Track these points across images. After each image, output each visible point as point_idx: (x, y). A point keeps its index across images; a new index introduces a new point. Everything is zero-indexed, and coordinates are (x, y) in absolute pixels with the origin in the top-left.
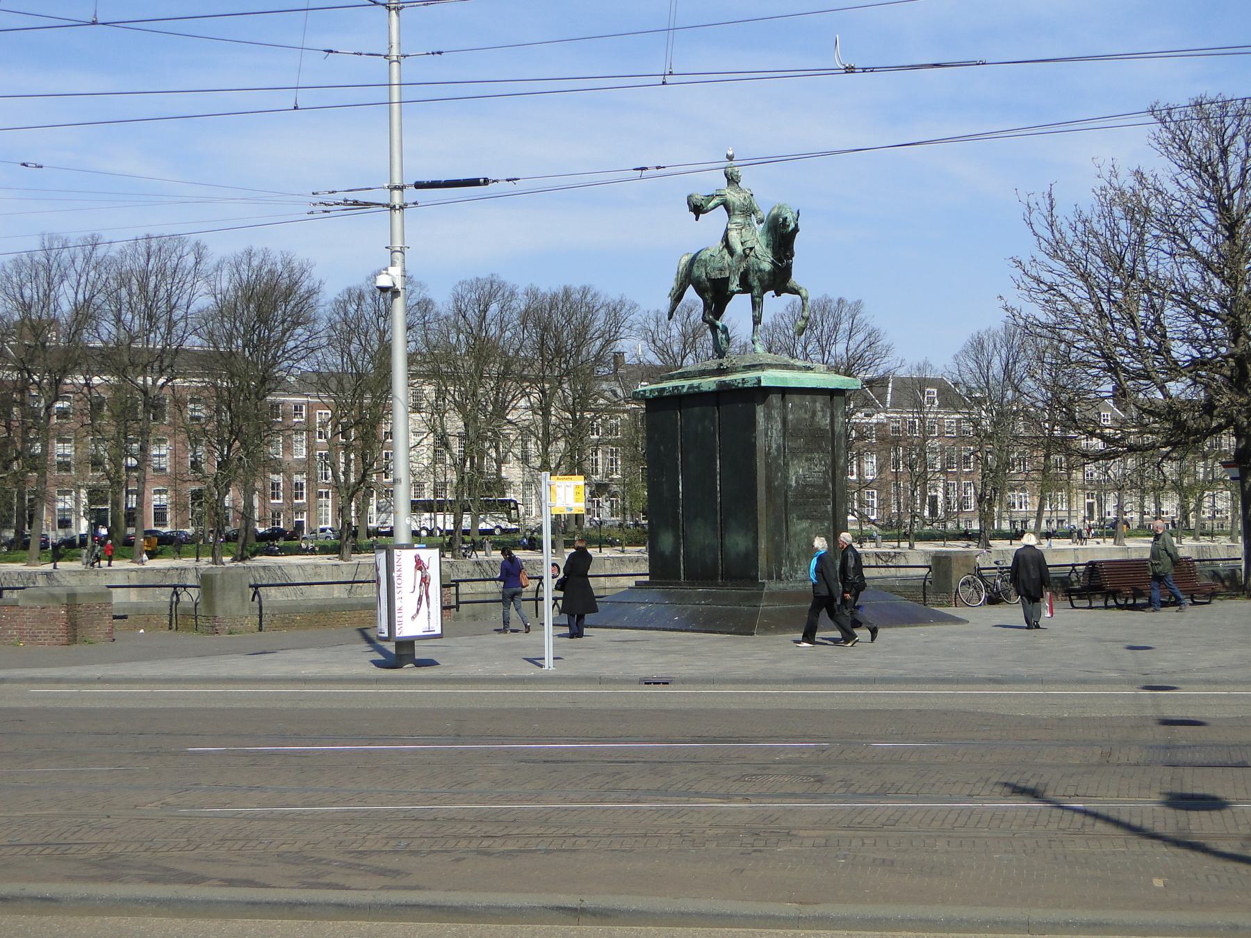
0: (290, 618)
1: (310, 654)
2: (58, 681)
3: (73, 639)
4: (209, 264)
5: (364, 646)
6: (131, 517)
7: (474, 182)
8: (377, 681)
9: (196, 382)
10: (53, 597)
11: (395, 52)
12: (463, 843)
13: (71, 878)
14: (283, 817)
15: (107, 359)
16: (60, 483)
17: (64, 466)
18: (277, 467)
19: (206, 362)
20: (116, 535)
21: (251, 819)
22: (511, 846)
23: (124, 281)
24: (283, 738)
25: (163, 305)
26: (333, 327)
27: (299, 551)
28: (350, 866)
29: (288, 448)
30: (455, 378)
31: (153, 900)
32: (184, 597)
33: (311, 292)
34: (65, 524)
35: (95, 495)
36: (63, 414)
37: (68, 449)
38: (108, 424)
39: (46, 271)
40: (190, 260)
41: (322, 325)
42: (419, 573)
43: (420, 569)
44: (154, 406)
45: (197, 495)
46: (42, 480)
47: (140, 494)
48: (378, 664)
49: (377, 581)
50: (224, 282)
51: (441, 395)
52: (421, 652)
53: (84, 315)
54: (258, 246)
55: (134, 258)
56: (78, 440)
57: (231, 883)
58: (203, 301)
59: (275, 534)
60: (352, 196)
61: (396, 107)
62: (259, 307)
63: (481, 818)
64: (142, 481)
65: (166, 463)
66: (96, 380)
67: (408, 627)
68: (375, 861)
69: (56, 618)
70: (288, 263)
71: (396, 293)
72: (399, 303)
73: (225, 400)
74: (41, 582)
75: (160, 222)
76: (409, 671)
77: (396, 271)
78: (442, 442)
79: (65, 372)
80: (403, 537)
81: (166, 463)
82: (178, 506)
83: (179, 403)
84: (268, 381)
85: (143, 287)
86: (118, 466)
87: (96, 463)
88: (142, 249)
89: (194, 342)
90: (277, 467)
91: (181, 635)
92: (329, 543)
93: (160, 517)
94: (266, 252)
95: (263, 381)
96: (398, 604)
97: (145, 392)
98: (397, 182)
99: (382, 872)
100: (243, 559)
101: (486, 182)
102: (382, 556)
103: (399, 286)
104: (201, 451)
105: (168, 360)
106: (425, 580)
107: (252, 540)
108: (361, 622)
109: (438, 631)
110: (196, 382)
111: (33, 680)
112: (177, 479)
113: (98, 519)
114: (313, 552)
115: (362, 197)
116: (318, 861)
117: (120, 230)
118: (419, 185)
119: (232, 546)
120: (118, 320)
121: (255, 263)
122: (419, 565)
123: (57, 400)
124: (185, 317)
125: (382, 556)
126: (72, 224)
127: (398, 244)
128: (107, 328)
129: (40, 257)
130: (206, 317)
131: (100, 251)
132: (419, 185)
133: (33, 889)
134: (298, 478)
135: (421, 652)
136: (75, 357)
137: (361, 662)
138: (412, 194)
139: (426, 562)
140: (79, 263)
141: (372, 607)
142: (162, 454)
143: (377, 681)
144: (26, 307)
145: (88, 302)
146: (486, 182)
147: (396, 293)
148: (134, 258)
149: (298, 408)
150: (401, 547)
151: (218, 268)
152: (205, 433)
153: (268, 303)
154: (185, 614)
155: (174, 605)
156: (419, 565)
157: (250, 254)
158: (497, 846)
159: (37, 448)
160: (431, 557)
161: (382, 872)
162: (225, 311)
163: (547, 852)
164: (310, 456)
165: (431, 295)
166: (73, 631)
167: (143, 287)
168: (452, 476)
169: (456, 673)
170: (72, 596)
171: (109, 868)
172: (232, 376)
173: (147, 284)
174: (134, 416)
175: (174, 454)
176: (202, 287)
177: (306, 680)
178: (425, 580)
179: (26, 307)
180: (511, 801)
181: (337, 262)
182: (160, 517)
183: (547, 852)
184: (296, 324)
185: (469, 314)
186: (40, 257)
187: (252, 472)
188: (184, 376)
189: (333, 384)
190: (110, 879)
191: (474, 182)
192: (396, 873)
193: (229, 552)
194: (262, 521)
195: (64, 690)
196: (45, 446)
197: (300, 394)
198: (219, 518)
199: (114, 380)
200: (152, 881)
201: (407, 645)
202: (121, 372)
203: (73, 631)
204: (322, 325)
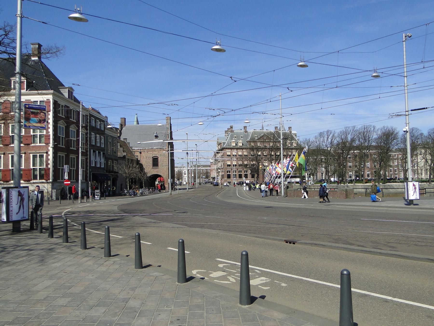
0: (389, 195)
1: (392, 202)
2: (342, 205)
3: (347, 198)
4: (376, 129)
5: (404, 201)
6: (362, 176)
7: (424, 108)
8: (405, 208)
9: (374, 151)
10: (343, 190)
11: (406, 85)
12: (412, 242)
13: (329, 242)
14: (375, 234)
15: (357, 148)
16: (349, 170)
17: (350, 167)
18: (391, 166)
19: (375, 147)
20: (360, 178)
21: (369, 233)
22: (423, 244)
23: (360, 133)
24: (380, 218)
25: (367, 138)
26: (402, 140)
27: (396, 182)
28: (385, 245)
29: (393, 163)
30: (429, 148)
31: (343, 248)
32: (368, 191)
33: (397, 133)
34: (351, 177)
35: (356, 172)
36: (350, 158)
37: (351, 164)
38: (358, 159)
39: (346, 133)
40: (373, 129)
41: (399, 139)
42: (20, 197)
43: (20, 196)
44: (366, 155)
45: (375, 172)
46: (346, 169)
47: (364, 172)
48: (406, 204)
49: (405, 188)
50: (379, 133)
51: (426, 152)
52: (415, 202)
53: (353, 140)
54: (386, 125)
55: (362, 129)
56: (352, 162)
57: (359, 246)
58: (375, 136)
59: (391, 179)
60: (397, 114)
61: (406, 94)
62: (386, 136)
63: (418, 237)
64: (364, 169)
65: (369, 166)
66: (355, 152)
67: (411, 198)
68: (390, 244)
69: (343, 194)
70: (392, 128)
71: (407, 132)
72: (408, 134)
73: (379, 154)
74: (346, 187)
75: (366, 122)
76: (412, 206)
77: (407, 128)
78: (426, 161)
79: (349, 150)
80: (410, 179)
81: (369, 166)
82: (372, 174)
83: (371, 155)
84: (388, 150)
85: (364, 134)
86: (360, 167)
87: (356, 166)
88: (363, 128)
89: (374, 144)
90: (391, 166)
91: (367, 197)
92: (402, 181)
93: (368, 176)
94: (387, 127)
95: (387, 150)
96: (409, 193)
97: (364, 153)
98: (407, 110)
99: (391, 247)
100: (384, 183)
101: (427, 108)
102: (405, 183)
103: (408, 130)
104: (376, 164)
105: (369, 148)
106: (415, 188)
107: (386, 180)
108: (402, 195)
109: (418, 198)
110: (374, 151)
111: (338, 205)
112: (371, 169)
113: (357, 176)
114: (399, 182)
115: (399, 114)
116: (378, 243)
117: (359, 125)
118: (412, 110)
119: (382, 181)
120: (359, 141)
121: (385, 128)
122: (414, 185)
123: (348, 155)
124: (372, 140)
125: (405, 183)
126: (350, 124)
127: (407, 122)
128: (357, 142)
129: (345, 131)
130: (376, 139)
131: (355, 129)
132: (412, 110)
133: (321, 243)
134: (395, 168)
135: (415, 202)
136: (352, 148)
137: (402, 204)
138: (410, 112)
139: (23, 193)
140: (352, 131)
141: (404, 193)
142: (368, 164)
143: (405, 208)
144: (342, 139)
145: (353, 138)
146: (427, 108)
147: (407, 132)
148: (362, 129)
149: (395, 155)
150: (410, 182)
151: (378, 130)
152: (376, 160)
153: (388, 136)
154: (368, 194)
155: (366, 192)
156: (414, 185)
157: (384, 127)
158: (420, 244)
159: (345, 164)
160: (417, 184)
161: (391, 247)
162: (380, 138)
163: (431, 246)
164: (398, 164)
165: (423, 132)
166: (347, 196)
167: (364, 134)
168: (428, 168)
169: (422, 207)
170: (346, 190)
171: (337, 241)
172: (381, 150)
173: (365, 134)
174: (363, 158)
175: (371, 164)
176: (375, 134)
177: (390, 207)
178: (415, 188)
179: (342, 139)
180: (426, 234)
181: (401, 127)
182: (368, 176)
183: (431, 246)
184: (394, 139)
185: (432, 135)
186: (345, 131)
187: (386, 167)
188: (372, 150)
189: (402, 150)
190: (336, 243)
191: (424, 108)
192: (394, 247)
193: (381, 182)
194: (388, 176)
195: (343, 207)
196: (346, 164)
197: (395, 152)
198: (380, 176)
199: (358, 151)
200: (344, 244)
201: (412, 201)
202: (360, 150)
203: (347, 196)
204: (399, 139)
